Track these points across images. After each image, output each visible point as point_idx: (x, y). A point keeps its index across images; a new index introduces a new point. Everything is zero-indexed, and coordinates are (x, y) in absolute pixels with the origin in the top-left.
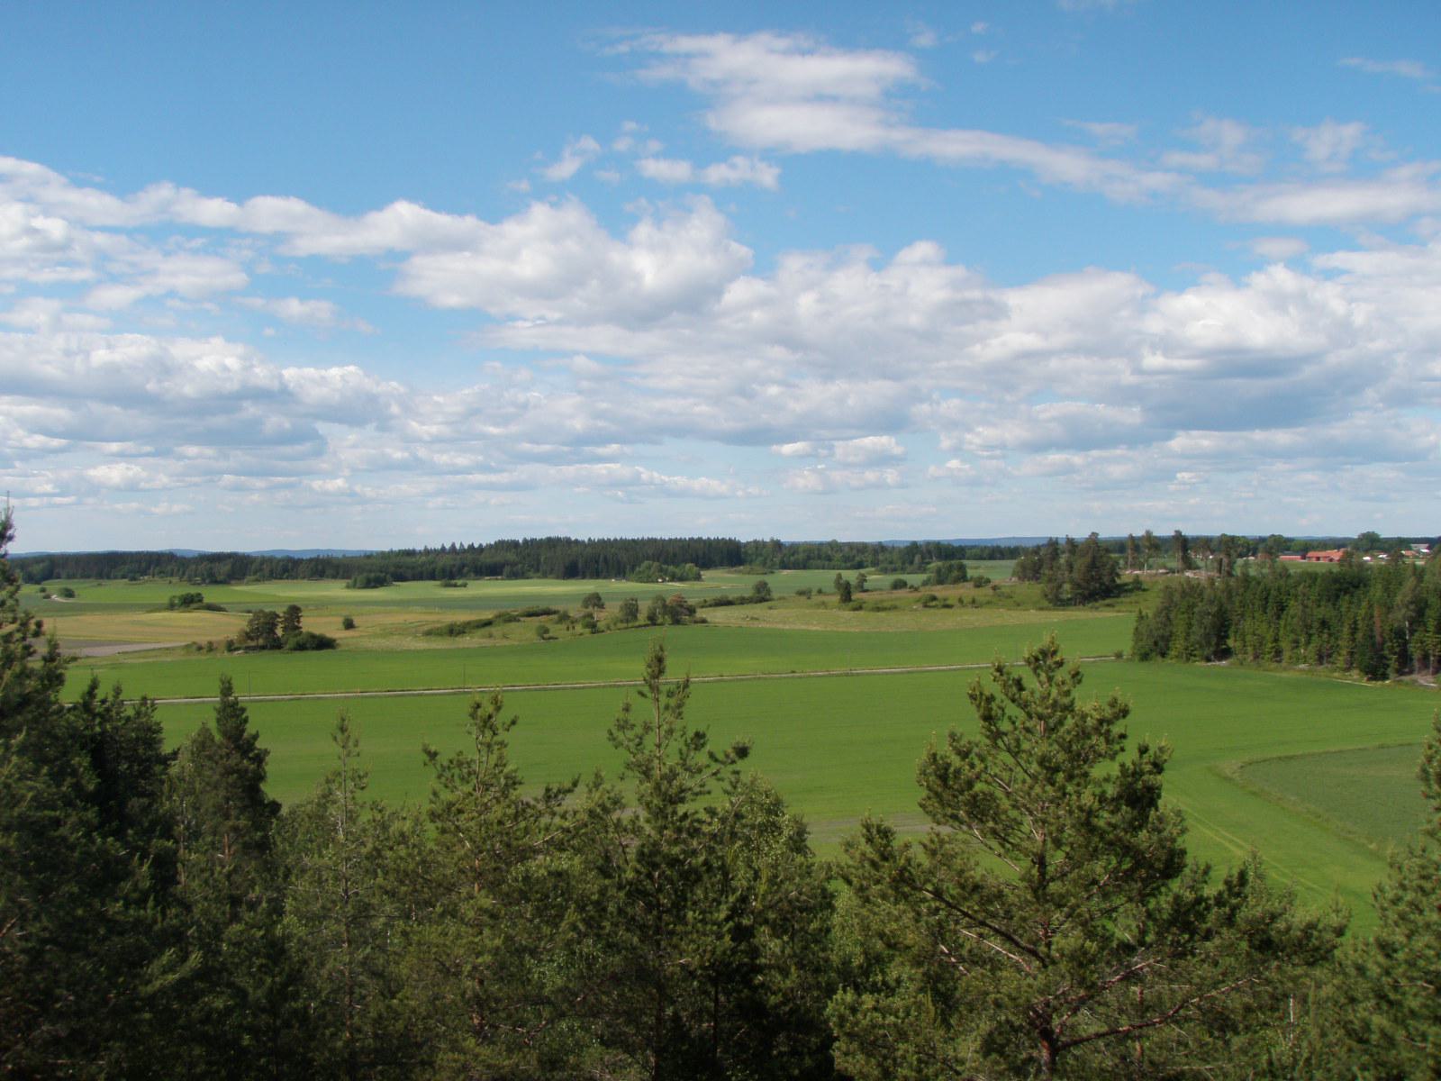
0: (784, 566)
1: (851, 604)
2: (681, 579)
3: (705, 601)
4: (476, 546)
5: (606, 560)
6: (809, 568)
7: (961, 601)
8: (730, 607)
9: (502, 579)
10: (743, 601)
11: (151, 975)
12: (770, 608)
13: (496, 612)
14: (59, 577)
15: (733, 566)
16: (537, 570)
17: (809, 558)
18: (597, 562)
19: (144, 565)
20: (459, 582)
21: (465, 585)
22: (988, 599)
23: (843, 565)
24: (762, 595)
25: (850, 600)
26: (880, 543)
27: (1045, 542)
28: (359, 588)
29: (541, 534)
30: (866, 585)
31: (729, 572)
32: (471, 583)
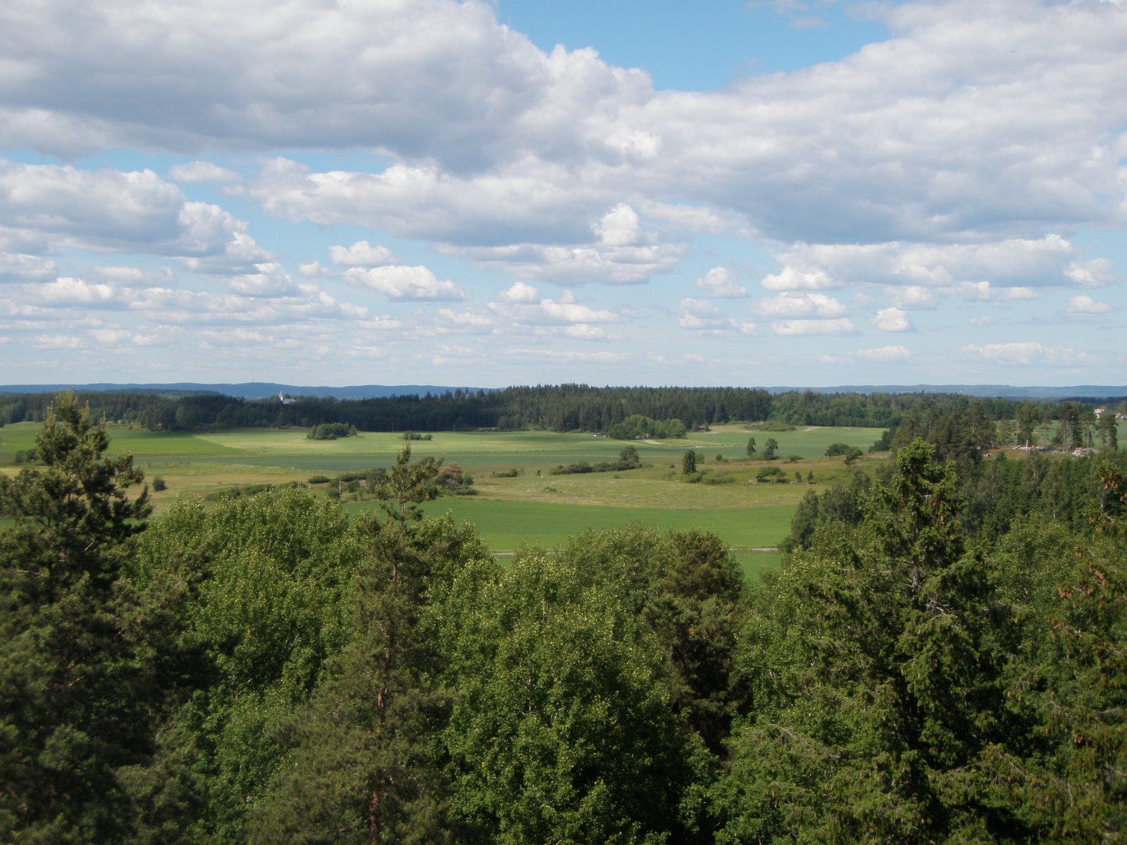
0: (810, 422)
1: (694, 476)
2: (662, 436)
3: (561, 467)
4: (433, 395)
5: (609, 409)
6: (840, 425)
7: (798, 476)
8: (588, 474)
9: (496, 431)
10: (604, 468)
11: (572, 742)
12: (617, 477)
13: (312, 475)
14: (30, 419)
15: (754, 420)
16: (537, 421)
17: (839, 414)
18: (600, 414)
19: (119, 407)
20: (423, 435)
21: (429, 438)
22: (833, 473)
23: (877, 422)
24: (628, 463)
25: (694, 470)
26: (809, 389)
27: (788, 391)
28: (318, 439)
29: (556, 381)
30: (776, 453)
31: (746, 428)
32: (436, 436)
